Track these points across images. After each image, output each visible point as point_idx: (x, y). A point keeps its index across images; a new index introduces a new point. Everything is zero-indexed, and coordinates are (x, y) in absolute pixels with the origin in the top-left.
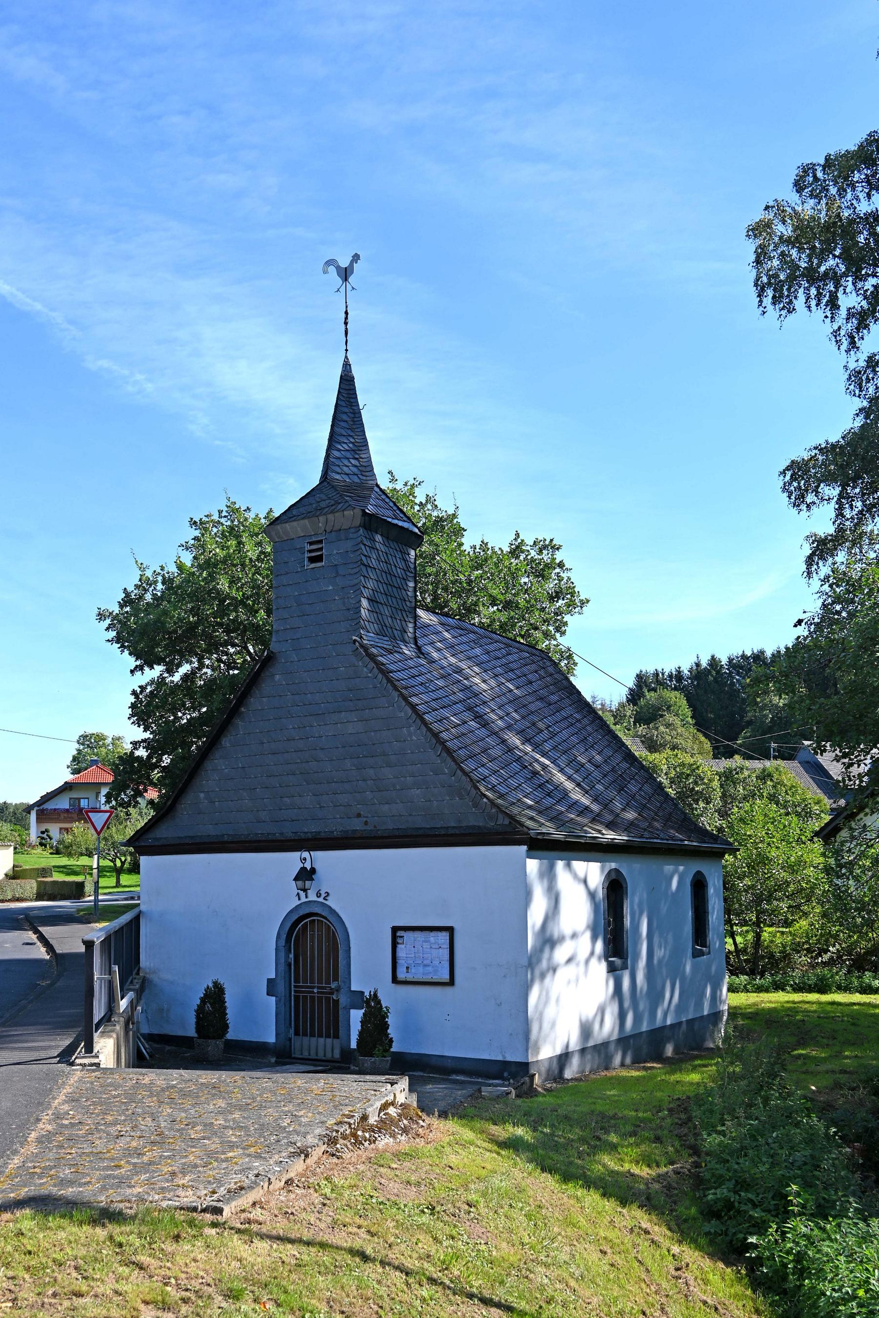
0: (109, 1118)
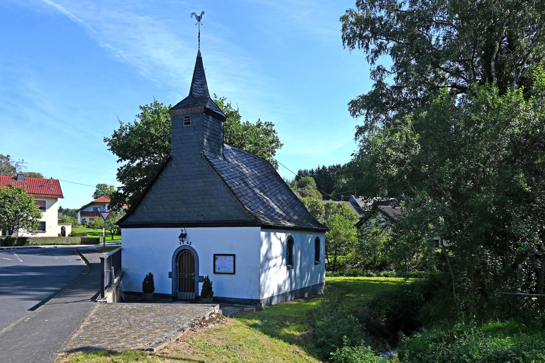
0: (111, 320)
